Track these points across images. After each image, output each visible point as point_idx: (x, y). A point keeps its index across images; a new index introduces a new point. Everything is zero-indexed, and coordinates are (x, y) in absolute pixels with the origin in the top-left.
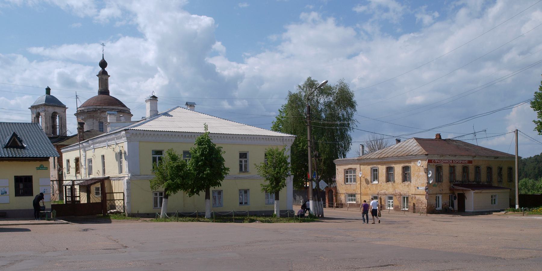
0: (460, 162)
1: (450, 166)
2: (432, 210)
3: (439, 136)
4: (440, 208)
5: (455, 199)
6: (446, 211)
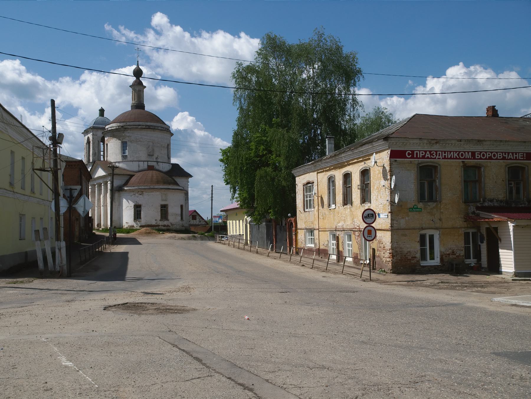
0: (499, 156)
1: (466, 168)
2: (405, 265)
3: (493, 111)
4: (436, 261)
5: (482, 242)
6: (453, 267)
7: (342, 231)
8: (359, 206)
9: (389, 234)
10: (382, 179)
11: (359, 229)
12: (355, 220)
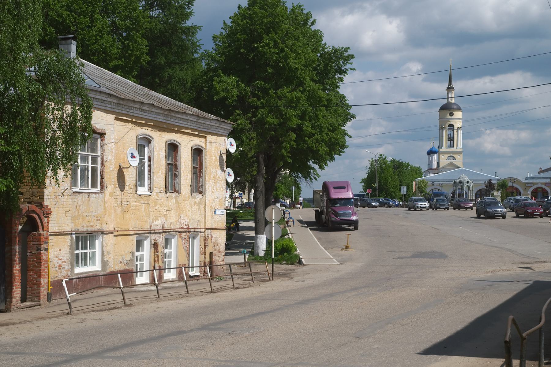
7: (160, 233)
8: (189, 197)
9: (224, 233)
10: (219, 168)
11: (188, 228)
12: (182, 216)
